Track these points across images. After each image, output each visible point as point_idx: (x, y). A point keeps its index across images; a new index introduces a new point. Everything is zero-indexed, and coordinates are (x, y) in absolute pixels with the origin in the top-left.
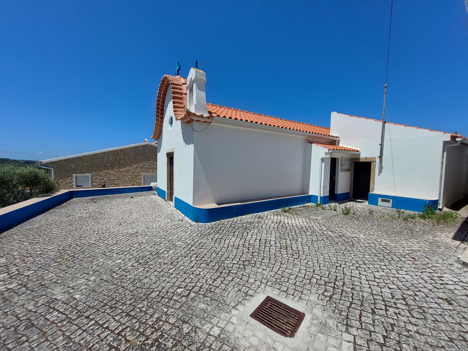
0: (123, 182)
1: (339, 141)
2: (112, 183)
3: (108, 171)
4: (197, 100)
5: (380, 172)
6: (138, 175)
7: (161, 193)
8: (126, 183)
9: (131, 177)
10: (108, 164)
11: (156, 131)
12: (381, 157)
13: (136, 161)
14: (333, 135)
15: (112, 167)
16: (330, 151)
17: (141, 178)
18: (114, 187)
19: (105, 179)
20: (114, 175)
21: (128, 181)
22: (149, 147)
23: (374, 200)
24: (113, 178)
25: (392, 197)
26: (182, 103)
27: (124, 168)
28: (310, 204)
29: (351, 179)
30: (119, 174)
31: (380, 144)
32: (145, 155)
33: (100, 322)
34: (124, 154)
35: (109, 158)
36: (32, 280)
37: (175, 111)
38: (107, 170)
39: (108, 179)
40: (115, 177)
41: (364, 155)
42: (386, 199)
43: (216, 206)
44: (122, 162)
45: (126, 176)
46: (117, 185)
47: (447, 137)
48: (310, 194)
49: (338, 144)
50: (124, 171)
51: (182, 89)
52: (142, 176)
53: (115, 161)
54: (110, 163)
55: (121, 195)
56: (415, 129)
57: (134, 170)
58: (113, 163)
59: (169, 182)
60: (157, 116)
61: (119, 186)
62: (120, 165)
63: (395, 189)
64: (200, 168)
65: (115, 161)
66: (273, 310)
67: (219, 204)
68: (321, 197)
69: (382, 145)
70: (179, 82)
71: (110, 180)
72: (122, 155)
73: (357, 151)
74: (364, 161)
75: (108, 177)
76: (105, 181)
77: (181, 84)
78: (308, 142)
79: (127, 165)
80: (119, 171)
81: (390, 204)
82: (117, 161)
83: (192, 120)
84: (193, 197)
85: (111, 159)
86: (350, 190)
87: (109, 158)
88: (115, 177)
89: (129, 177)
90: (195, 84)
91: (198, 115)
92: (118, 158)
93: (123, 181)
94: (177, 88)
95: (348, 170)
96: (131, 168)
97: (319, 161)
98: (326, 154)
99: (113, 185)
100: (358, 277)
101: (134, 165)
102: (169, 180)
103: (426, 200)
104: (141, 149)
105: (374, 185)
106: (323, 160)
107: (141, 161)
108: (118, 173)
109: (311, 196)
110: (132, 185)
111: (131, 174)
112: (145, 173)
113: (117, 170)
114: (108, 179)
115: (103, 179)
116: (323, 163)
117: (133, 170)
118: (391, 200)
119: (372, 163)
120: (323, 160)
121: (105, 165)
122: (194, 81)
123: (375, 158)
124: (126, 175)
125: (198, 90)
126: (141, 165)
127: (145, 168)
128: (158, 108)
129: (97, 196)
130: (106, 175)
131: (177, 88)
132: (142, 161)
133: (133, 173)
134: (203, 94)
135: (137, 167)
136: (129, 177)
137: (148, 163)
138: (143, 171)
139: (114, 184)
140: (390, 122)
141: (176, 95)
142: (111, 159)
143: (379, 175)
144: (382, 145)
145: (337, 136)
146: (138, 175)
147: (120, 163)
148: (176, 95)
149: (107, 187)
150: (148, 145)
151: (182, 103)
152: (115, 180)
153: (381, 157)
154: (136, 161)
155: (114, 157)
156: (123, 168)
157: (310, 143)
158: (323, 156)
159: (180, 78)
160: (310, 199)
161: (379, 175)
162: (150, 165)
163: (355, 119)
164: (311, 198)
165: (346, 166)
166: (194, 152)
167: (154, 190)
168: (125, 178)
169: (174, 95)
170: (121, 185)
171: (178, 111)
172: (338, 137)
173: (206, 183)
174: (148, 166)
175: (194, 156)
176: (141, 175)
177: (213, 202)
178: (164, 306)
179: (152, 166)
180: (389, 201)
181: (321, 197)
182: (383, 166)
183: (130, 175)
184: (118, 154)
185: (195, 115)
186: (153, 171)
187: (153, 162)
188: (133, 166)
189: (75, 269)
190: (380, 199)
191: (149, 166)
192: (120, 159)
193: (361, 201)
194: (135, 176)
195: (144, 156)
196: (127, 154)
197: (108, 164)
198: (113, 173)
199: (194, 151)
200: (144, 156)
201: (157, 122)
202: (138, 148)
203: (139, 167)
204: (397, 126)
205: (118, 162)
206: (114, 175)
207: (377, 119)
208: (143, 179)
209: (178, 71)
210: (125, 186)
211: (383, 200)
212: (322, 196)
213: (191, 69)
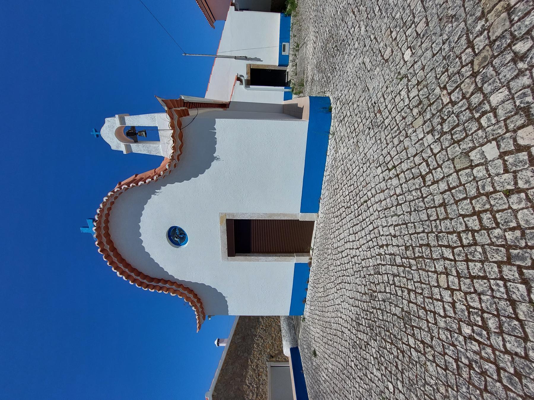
5: (259, 60)
12: (246, 58)
22: (218, 394)
25: (281, 42)
33: (525, 78)
42: (282, 48)
47: (232, 8)
69: (236, 58)
74: (249, 75)
81: (287, 44)
118: (283, 43)
123: (247, 65)
137: (248, 395)
143: (262, 61)
150: (213, 396)
153: (246, 58)
161: (262, 61)
162: (251, 391)
167: (297, 344)
178: (466, 102)
179: (253, 386)
180: (284, 45)
186: (263, 384)
187: (246, 385)
190: (283, 53)
191: (253, 393)
211: (284, 51)
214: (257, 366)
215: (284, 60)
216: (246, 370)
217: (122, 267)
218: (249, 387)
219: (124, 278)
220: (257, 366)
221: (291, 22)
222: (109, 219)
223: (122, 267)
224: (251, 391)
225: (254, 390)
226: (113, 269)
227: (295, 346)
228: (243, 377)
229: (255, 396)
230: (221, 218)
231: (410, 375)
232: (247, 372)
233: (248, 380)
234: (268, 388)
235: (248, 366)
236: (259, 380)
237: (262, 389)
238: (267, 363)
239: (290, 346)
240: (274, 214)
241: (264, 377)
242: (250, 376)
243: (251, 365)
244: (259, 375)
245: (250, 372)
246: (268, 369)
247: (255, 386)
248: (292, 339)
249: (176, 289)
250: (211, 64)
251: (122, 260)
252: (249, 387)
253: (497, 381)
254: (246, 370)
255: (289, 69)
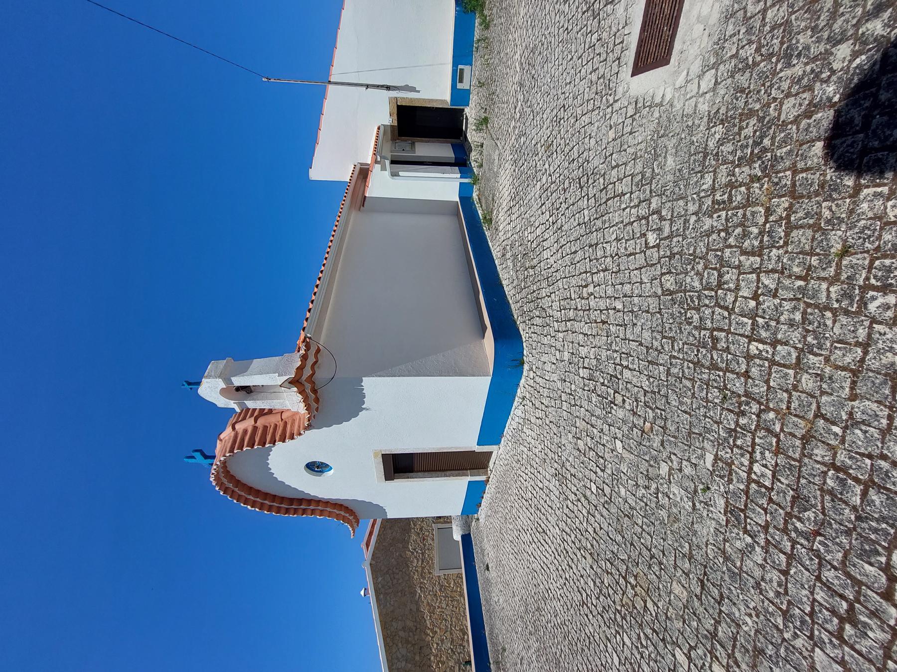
0: (457, 618)
1: (361, 164)
2: (461, 645)
3: (432, 658)
4: (268, 373)
5: (413, 89)
6: (439, 583)
7: (474, 497)
8: (459, 610)
9: (443, 599)
10: (417, 658)
11: (338, 517)
12: (388, 88)
13: (407, 589)
14: (349, 178)
15: (422, 648)
16: (379, 159)
17: (445, 575)
18: (468, 641)
19: (451, 663)
20: (442, 641)
21: (453, 606)
22: (377, 562)
23: (460, 96)
24: (449, 645)
25: (455, 64)
26: (276, 426)
27: (425, 616)
28: (475, 195)
29: (428, 142)
30: (438, 631)
31: (367, 88)
32: (394, 570)
34: (392, 621)
35: (403, 656)
36: (697, 629)
37: (292, 438)
38: (430, 659)
39: (451, 657)
40: (446, 638)
41: (386, 118)
42: (458, 76)
43: (489, 332)
44: (410, 624)
45: (443, 612)
46: (465, 633)
48: (458, 199)
49: (368, 165)
50: (430, 617)
51: (244, 430)
52: (441, 573)
53: (408, 642)
54: (415, 654)
55: (483, 602)
56: (340, 32)
57: (429, 594)
58: (413, 645)
59: (448, 473)
60: (304, 512)
61: (467, 627)
62: (419, 627)
63: (441, 64)
64: (411, 366)
65: (408, 642)
66: (660, 12)
67: (484, 329)
68: (461, 177)
69: (368, 86)
70: (230, 439)
71: (452, 650)
72: (394, 624)
73: (379, 128)
74: (395, 117)
75: (447, 658)
76: (456, 663)
77: (233, 434)
78: (363, 206)
79: (418, 610)
80: (432, 630)
81: (467, 69)
82: (409, 636)
83: (310, 379)
84: (474, 376)
85: (403, 651)
86: (447, 142)
87: (403, 656)
88: (446, 638)
89: (444, 606)
90: (234, 379)
91: (300, 363)
92: (401, 634)
93: (454, 619)
94: (243, 440)
95: (413, 144)
96: (426, 599)
97: (397, 181)
98: (383, 168)
99: (465, 644)
100: (619, 659)
101: (418, 594)
102: (443, 473)
103: (456, 11)
104: (380, 579)
105: (437, 100)
106: (394, 174)
107: (407, 578)
108: (436, 632)
109: (460, 198)
110: (462, 595)
111: (437, 600)
112: (433, 568)
113: (429, 635)
114: (451, 657)
115: (451, 669)
116: (401, 173)
117: (429, 597)
118: (460, 67)
119: (399, 104)
120: (394, 174)
121: (420, 667)
122: (228, 381)
123: (390, 99)
124: (440, 612)
125: (248, 372)
126: (415, 577)
127: (423, 568)
128: (287, 511)
129: (490, 663)
130: (443, 663)
131: (243, 440)
132: (409, 575)
133: (436, 595)
134: (257, 363)
135: (421, 588)
136: (444, 606)
137: (412, 562)
138: (430, 573)
139: (463, 639)
140: (328, 73)
141: (257, 440)
142: (403, 651)
143: (419, 92)
144: (368, 86)
145: (353, 166)
146: (439, 583)
147: (414, 629)
148: (257, 440)
149: (470, 656)
150: (371, 564)
151: (276, 426)
152: (453, 639)
153: (388, 88)
154: (407, 589)
155: (400, 645)
156: (425, 621)
157: (364, 201)
158: (387, 173)
159: (221, 440)
160: (466, 199)
161: (419, 92)
162: (416, 557)
163: (322, 135)
164: (464, 197)
165: (406, 145)
166: (380, 376)
167: (470, 530)
168: (446, 615)
169: (256, 443)
170: (464, 622)
171: (291, 430)
172: (355, 165)
173: (443, 356)
174: (418, 562)
175: (389, 376)
176: (439, 576)
177: (482, 344)
179: (417, 552)
180: (462, 71)
181: (461, 177)
182: (403, 85)
183: (440, 602)
184: (394, 634)
185: (300, 369)
186: (429, 549)
187: (409, 551)
188: (420, 596)
189: (652, 538)
190: (459, 86)
192: (404, 629)
193: (464, 120)
194: (440, 590)
195: (397, 571)
196: (393, 611)
197: (417, 658)
198: (438, 644)
199: (376, 376)
200: (397, 571)
201: (318, 512)
202: (380, 586)
203: (421, 583)
204: (336, 61)
205: (411, 634)
206: (442, 641)
207: (323, 95)
208: (447, 572)
209: (206, 457)
210: (464, 613)
211: (461, 81)
212: (459, 175)
213: (202, 395)
214: (421, 529)
215: (460, 96)
216: (408, 534)
217: (252, 498)
218: (413, 553)
219: (257, 510)
220: (421, 529)
221: (476, 37)
222: (228, 469)
223: (252, 498)
224: (416, 557)
225: (419, 556)
226: (242, 505)
227: (467, 533)
228: (405, 543)
229: (420, 563)
230: (376, 456)
231: (634, 420)
232: (410, 536)
233: (411, 546)
234: (435, 554)
235: (410, 529)
236: (425, 545)
237: (428, 555)
238: (433, 525)
239: (461, 533)
240: (443, 448)
241: (430, 542)
242: (414, 541)
243: (414, 529)
244: (424, 539)
245: (414, 537)
246: (434, 533)
247: (419, 551)
248: (464, 524)
249: (323, 509)
250: (321, 96)
251: (250, 490)
252: (413, 553)
253: (663, 569)
254: (408, 534)
255: (471, 113)
